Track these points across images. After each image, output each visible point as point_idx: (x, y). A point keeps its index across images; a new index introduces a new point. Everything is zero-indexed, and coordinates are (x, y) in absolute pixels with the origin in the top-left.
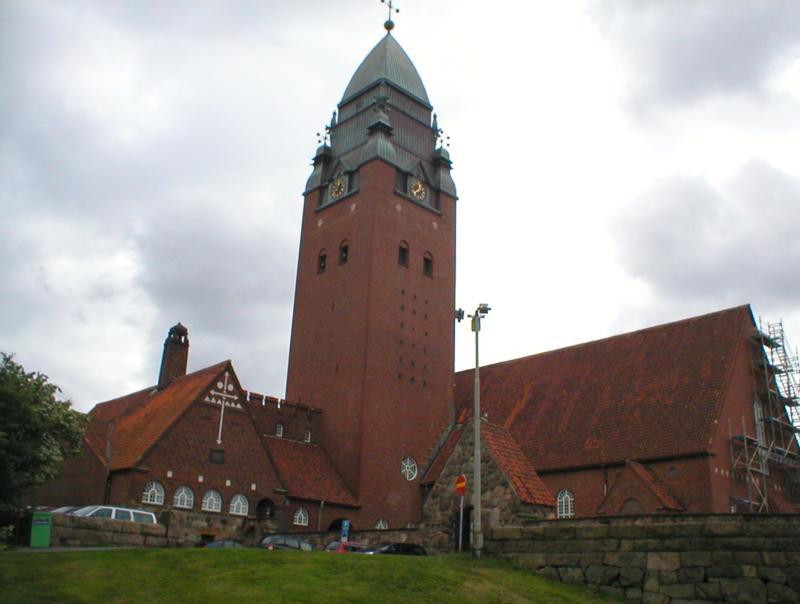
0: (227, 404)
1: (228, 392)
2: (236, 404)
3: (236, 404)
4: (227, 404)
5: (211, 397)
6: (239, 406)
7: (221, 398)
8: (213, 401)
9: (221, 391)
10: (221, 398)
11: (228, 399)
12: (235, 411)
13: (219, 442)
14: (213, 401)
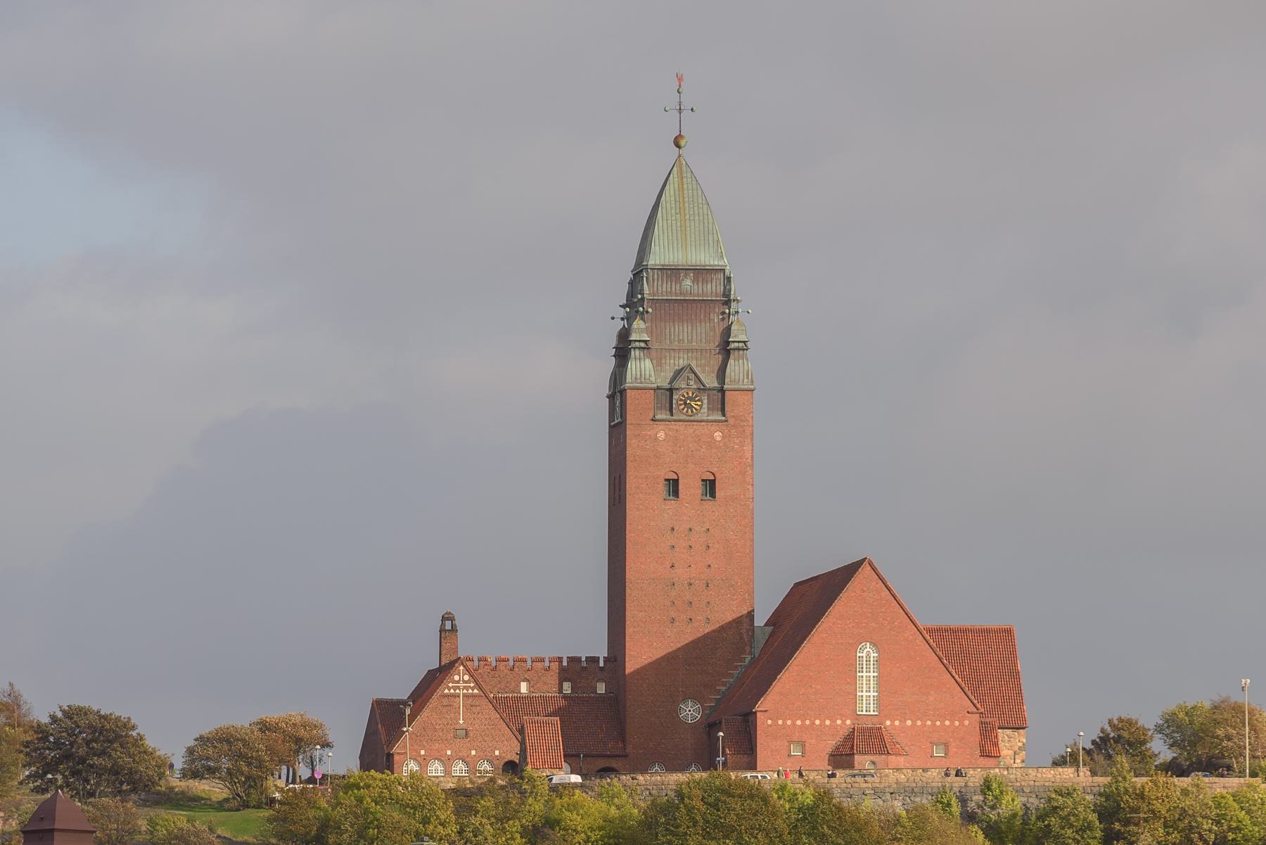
0: (465, 691)
1: (465, 682)
4: (465, 691)
6: (476, 691)
7: (458, 688)
8: (452, 691)
10: (458, 688)
12: (473, 696)
13: (461, 722)
14: (452, 691)
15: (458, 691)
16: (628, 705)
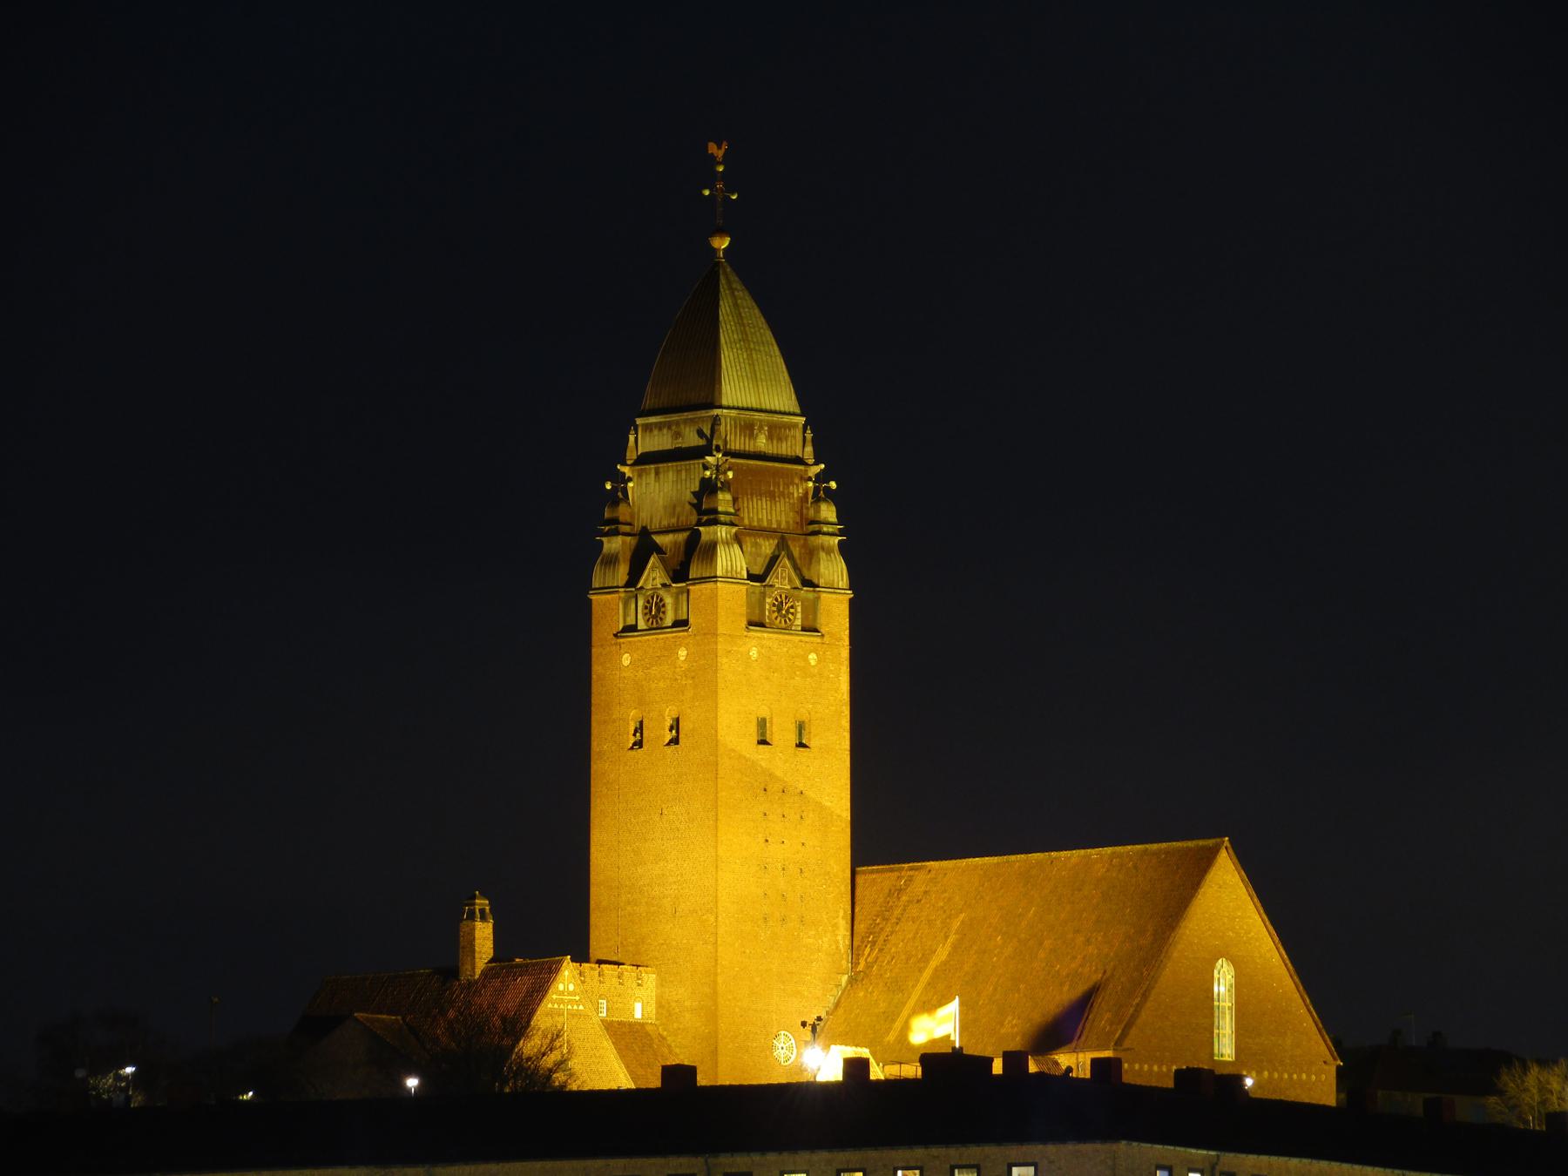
0: (570, 1007)
2: (578, 1005)
3: (578, 1005)
5: (553, 1003)
6: (581, 1007)
8: (556, 1006)
9: (562, 993)
11: (570, 1002)
14: (556, 1006)
15: (562, 1006)
16: (720, 1036)
